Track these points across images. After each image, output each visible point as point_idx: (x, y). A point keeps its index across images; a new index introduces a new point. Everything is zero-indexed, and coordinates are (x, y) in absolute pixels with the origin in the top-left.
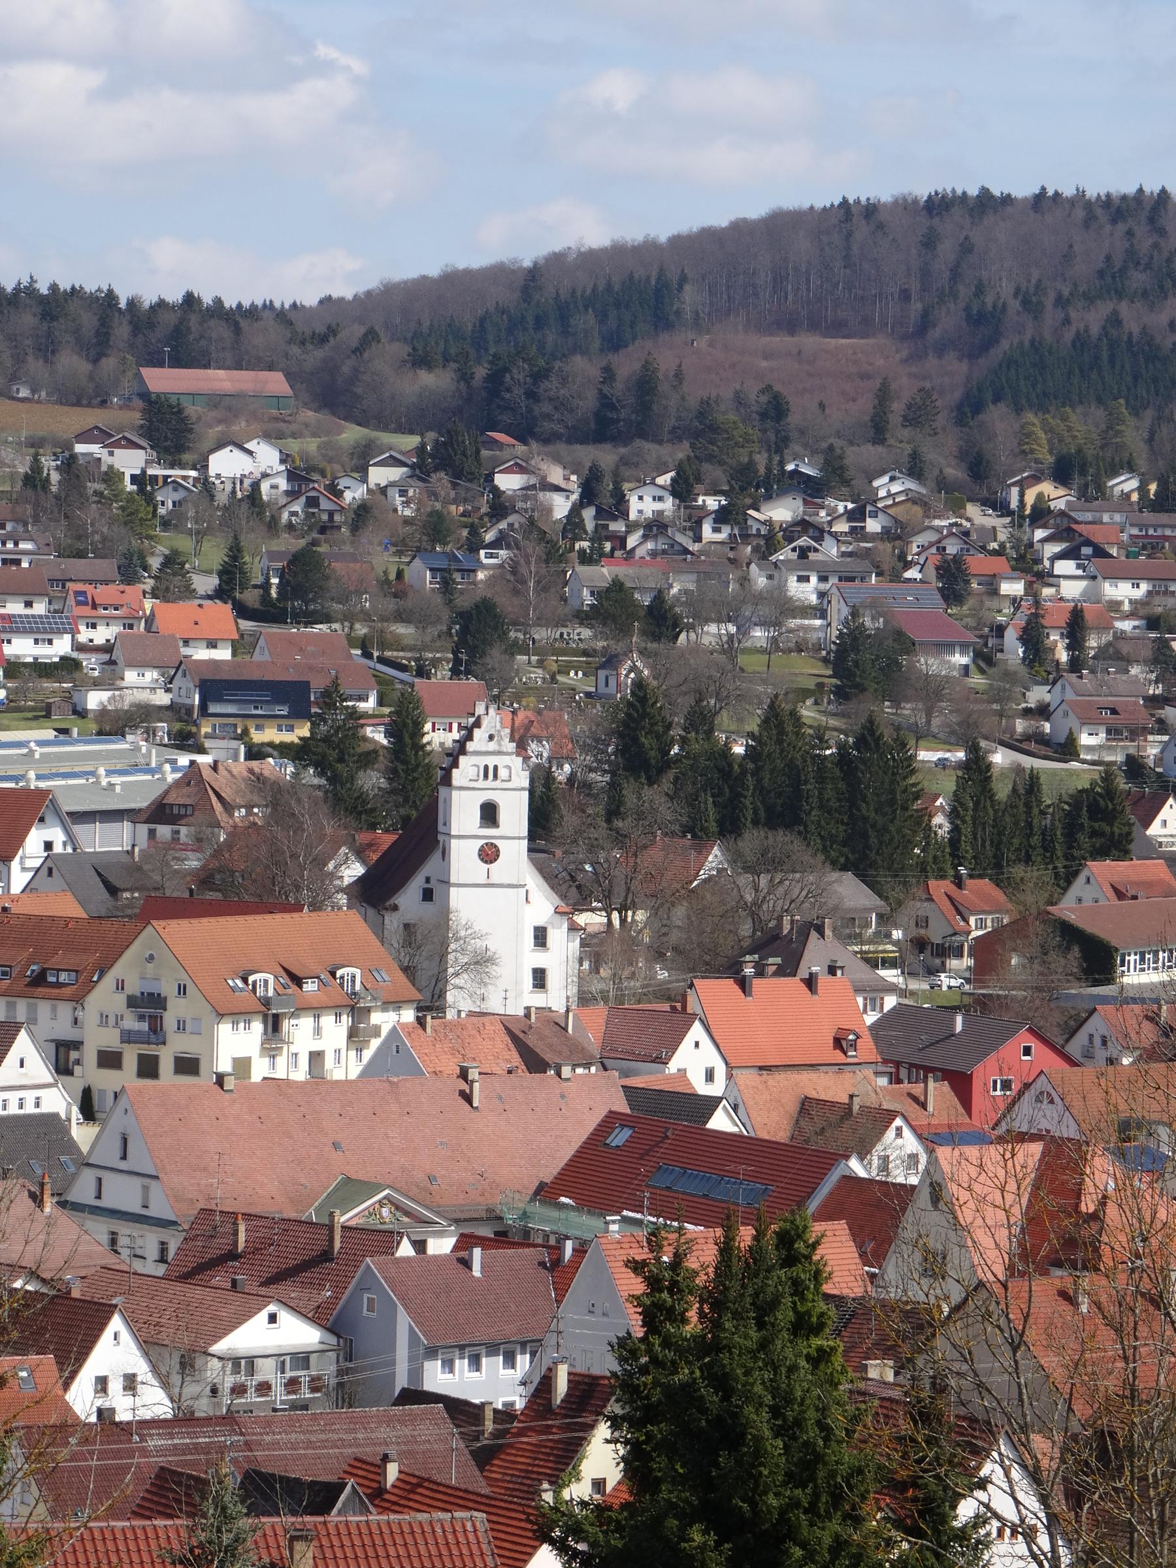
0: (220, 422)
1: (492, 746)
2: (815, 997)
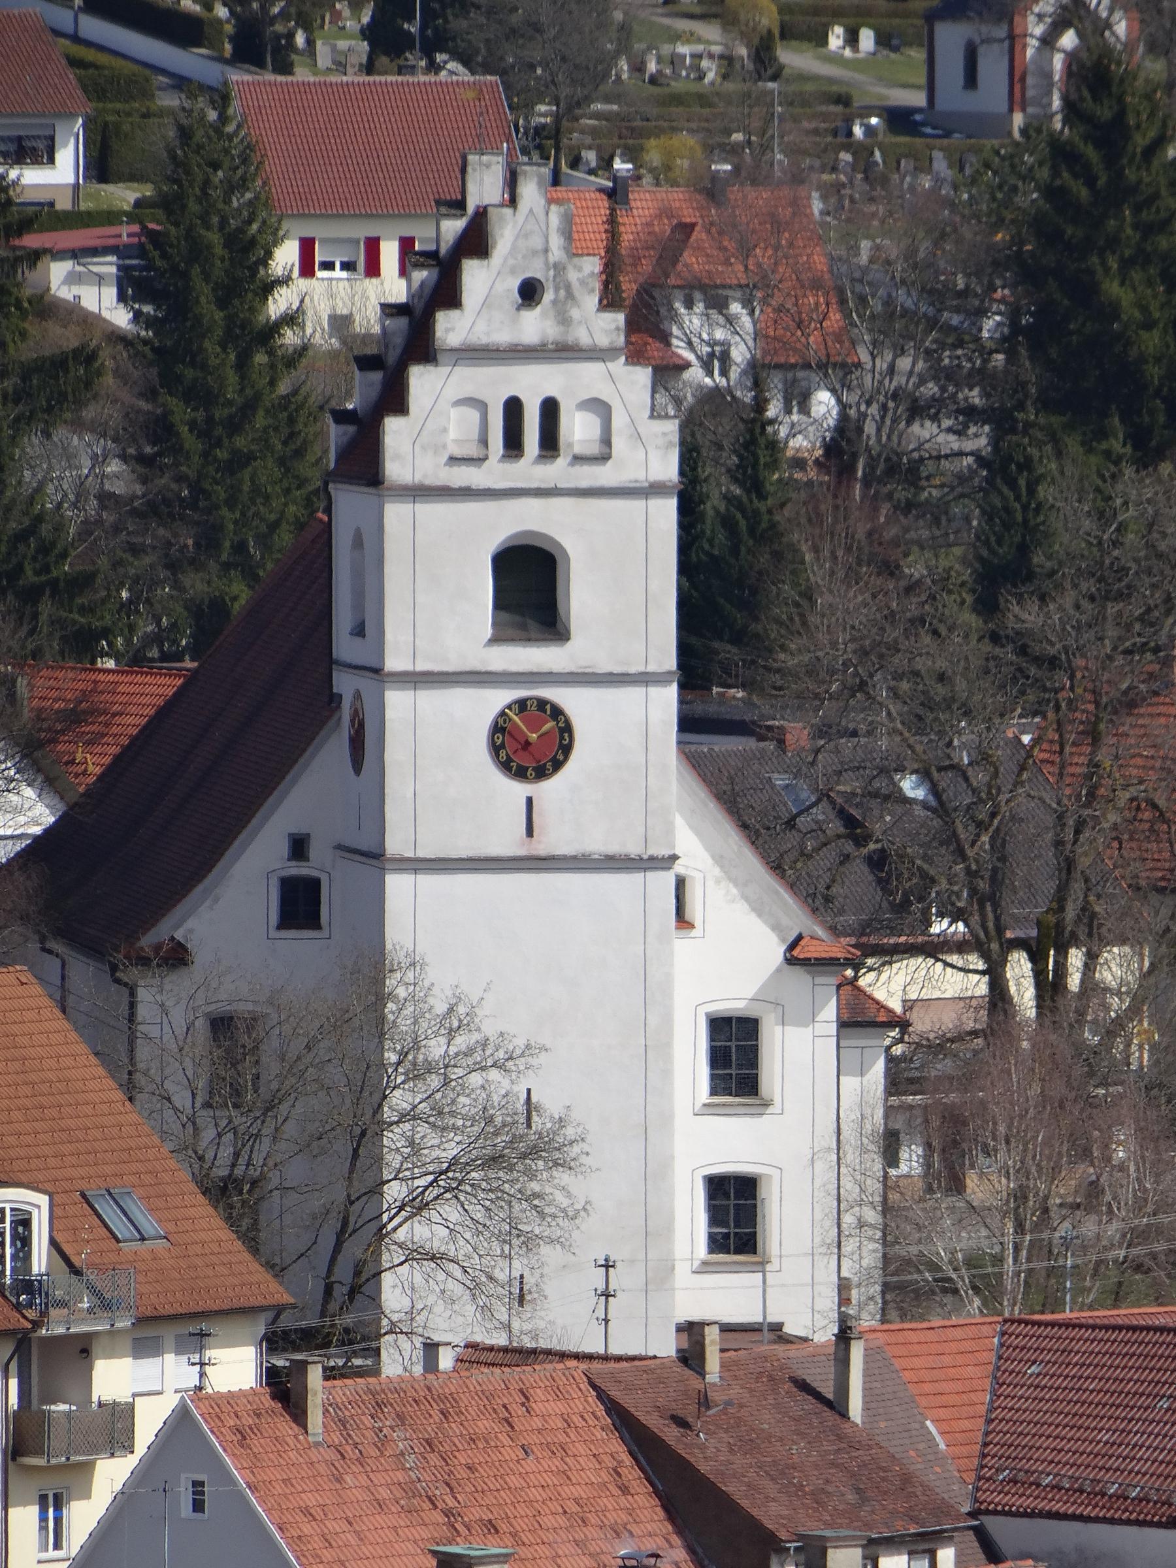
1: (534, 326)
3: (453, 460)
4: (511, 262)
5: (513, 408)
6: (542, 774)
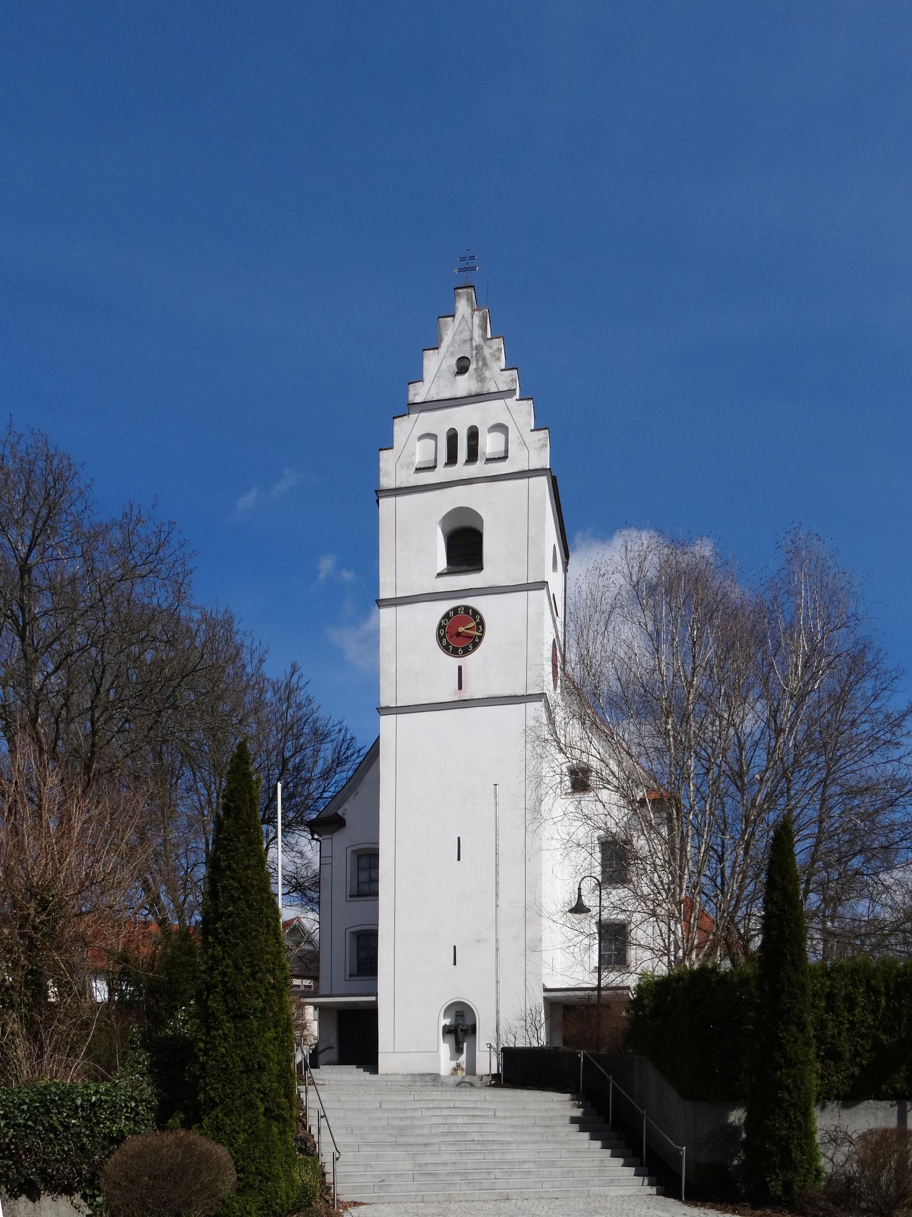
1: (465, 385)
2: (568, 1121)
3: (418, 470)
4: (451, 349)
5: (452, 437)
6: (466, 651)
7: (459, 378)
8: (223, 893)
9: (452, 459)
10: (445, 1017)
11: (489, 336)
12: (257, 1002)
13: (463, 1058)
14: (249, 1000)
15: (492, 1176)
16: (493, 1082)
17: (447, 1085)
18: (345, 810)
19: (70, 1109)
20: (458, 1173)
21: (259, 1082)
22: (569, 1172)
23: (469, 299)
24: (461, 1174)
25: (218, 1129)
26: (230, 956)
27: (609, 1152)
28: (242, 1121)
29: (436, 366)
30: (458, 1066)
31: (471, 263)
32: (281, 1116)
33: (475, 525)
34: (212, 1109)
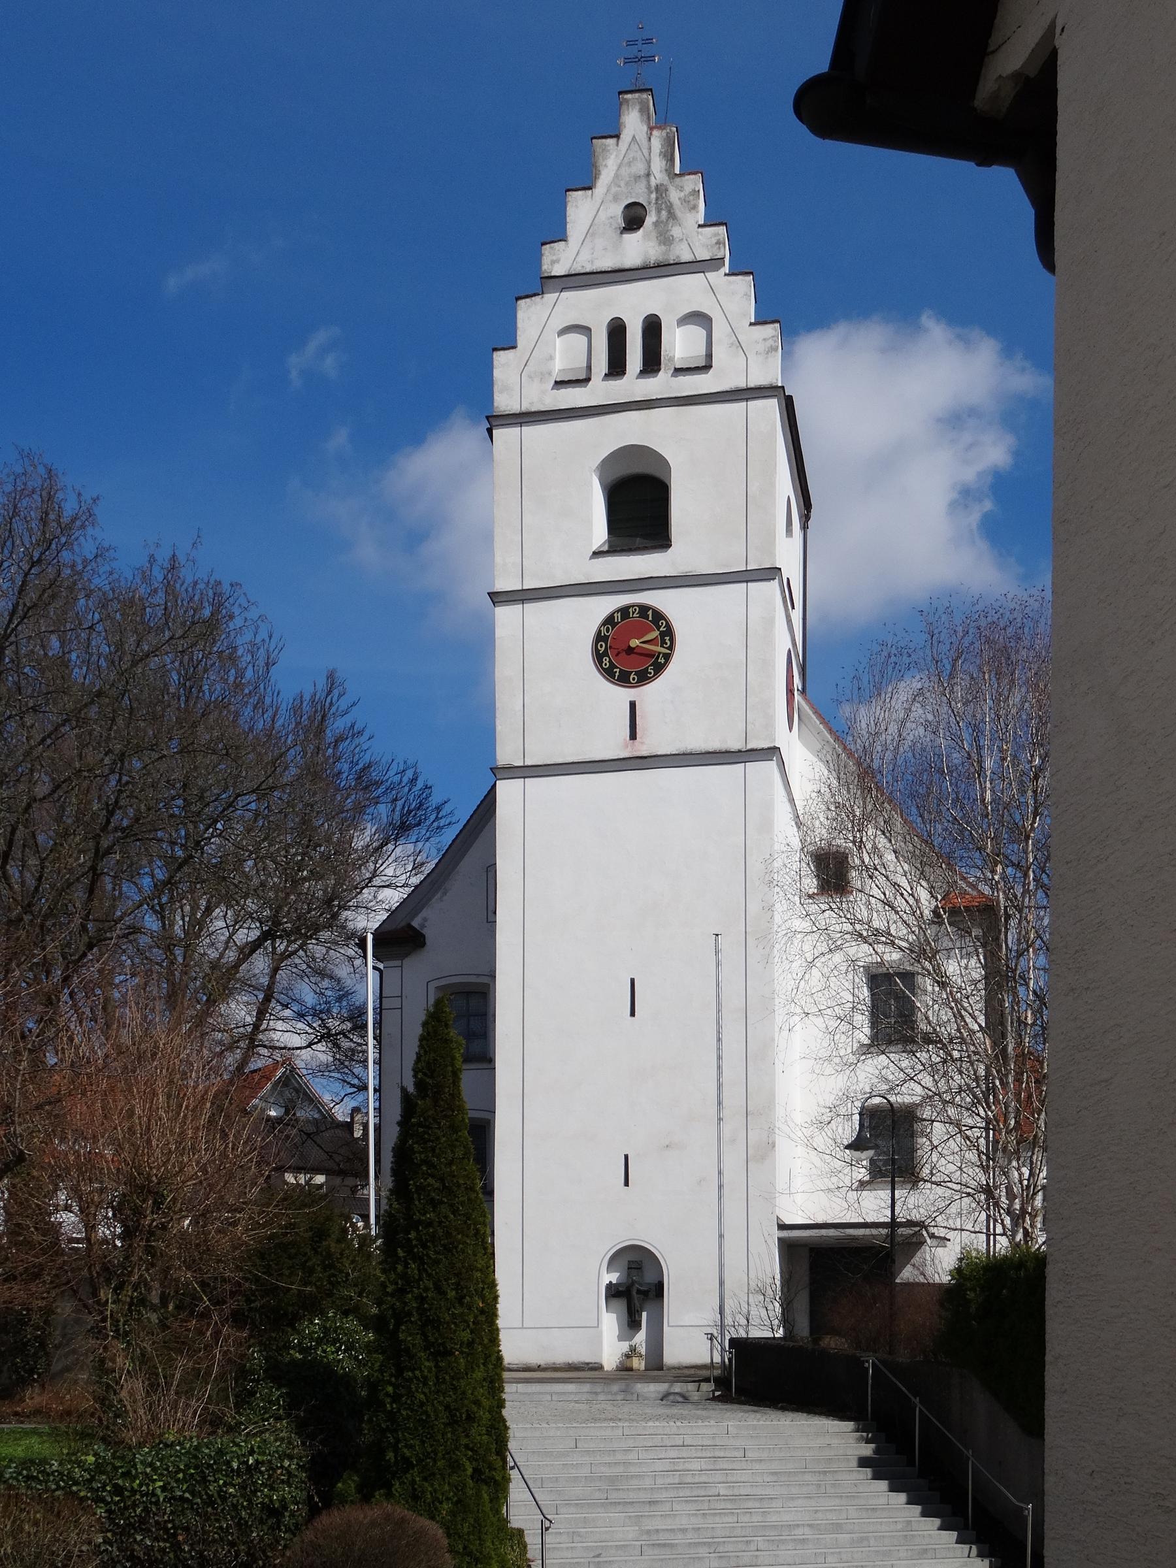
0: (980, 1026)
1: (637, 248)
2: (855, 1463)
3: (559, 384)
4: (614, 189)
5: (617, 331)
6: (644, 678)
7: (627, 236)
8: (419, 1195)
9: (617, 367)
10: (610, 1268)
11: (677, 171)
12: (463, 1334)
13: (641, 1337)
14: (455, 1331)
15: (753, 1547)
16: (717, 1393)
17: (646, 1399)
18: (425, 920)
19: (227, 1476)
20: (705, 1543)
21: (467, 1436)
22: (862, 1539)
23: (644, 110)
24: (709, 1544)
25: (415, 1498)
26: (429, 1275)
27: (917, 1509)
28: (446, 1487)
29: (589, 217)
30: (633, 1349)
31: (646, 50)
32: (493, 1478)
33: (657, 473)
34: (406, 1471)
